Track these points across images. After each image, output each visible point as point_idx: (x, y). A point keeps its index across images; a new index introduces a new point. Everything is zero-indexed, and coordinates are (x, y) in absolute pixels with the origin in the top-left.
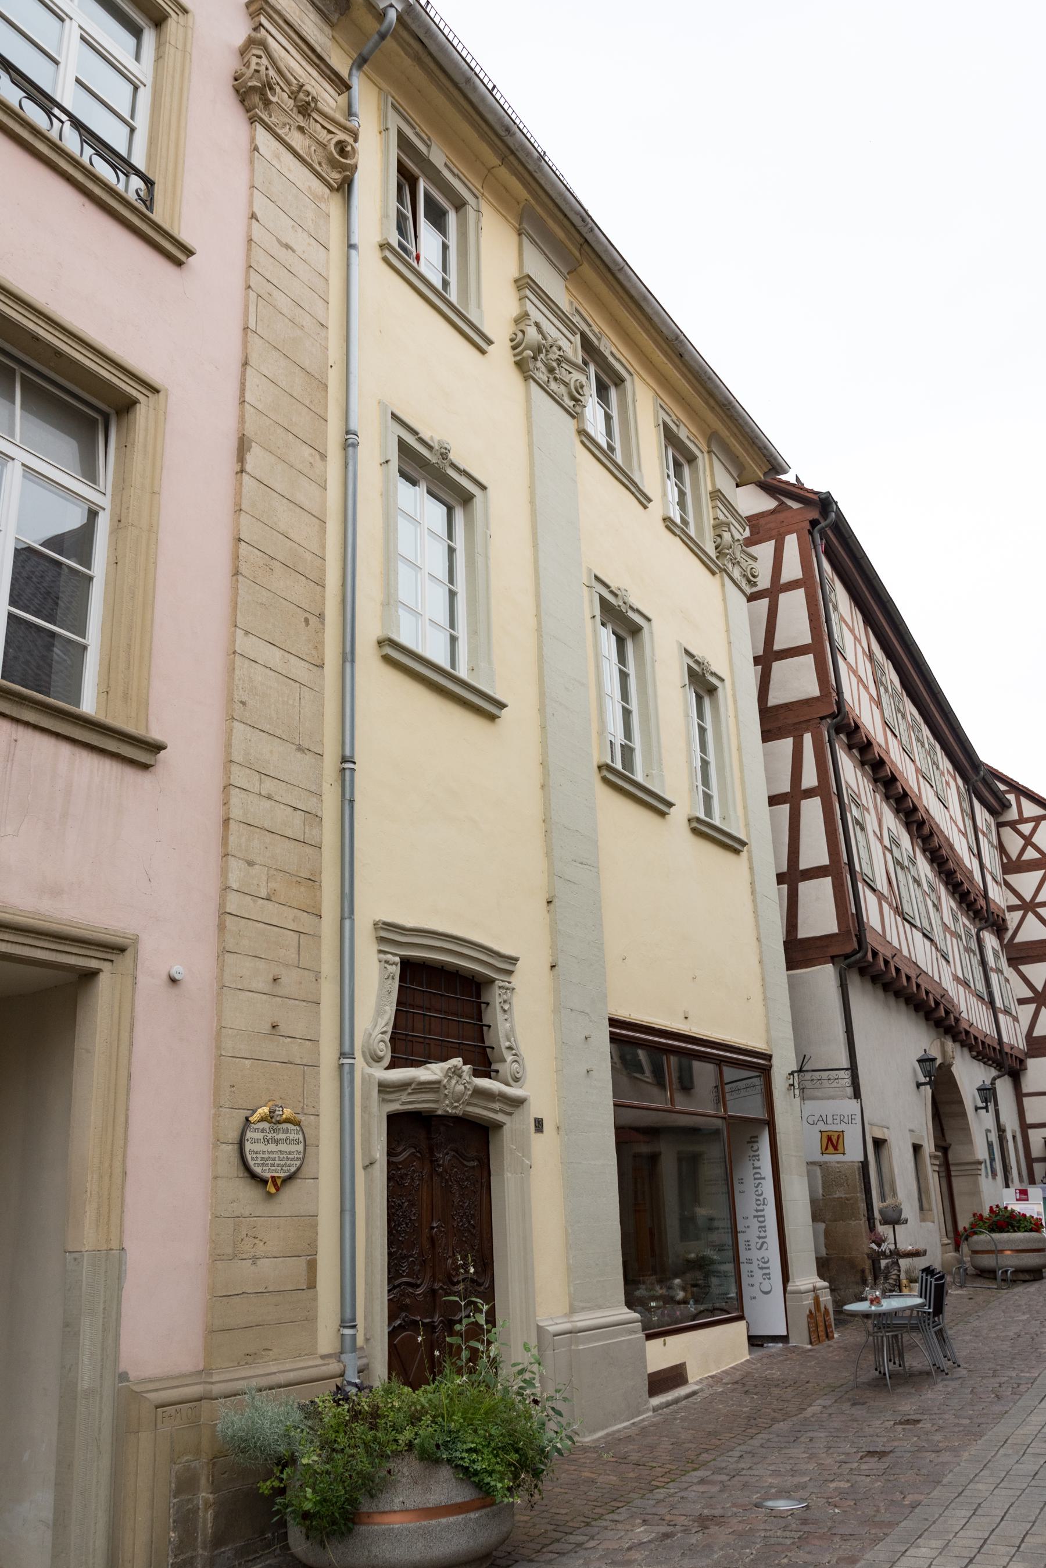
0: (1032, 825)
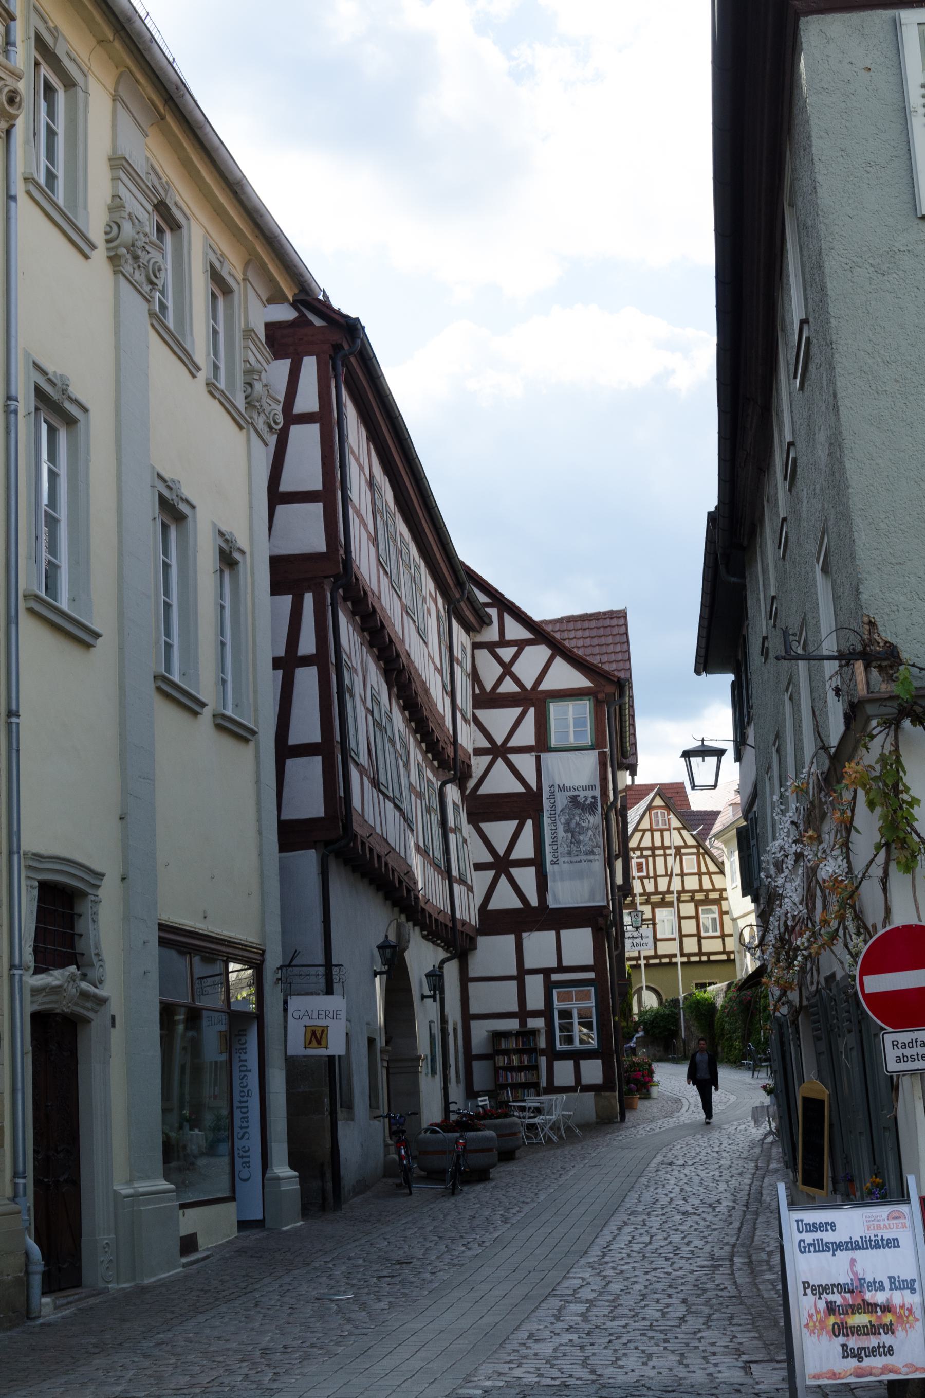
0: (514, 649)
